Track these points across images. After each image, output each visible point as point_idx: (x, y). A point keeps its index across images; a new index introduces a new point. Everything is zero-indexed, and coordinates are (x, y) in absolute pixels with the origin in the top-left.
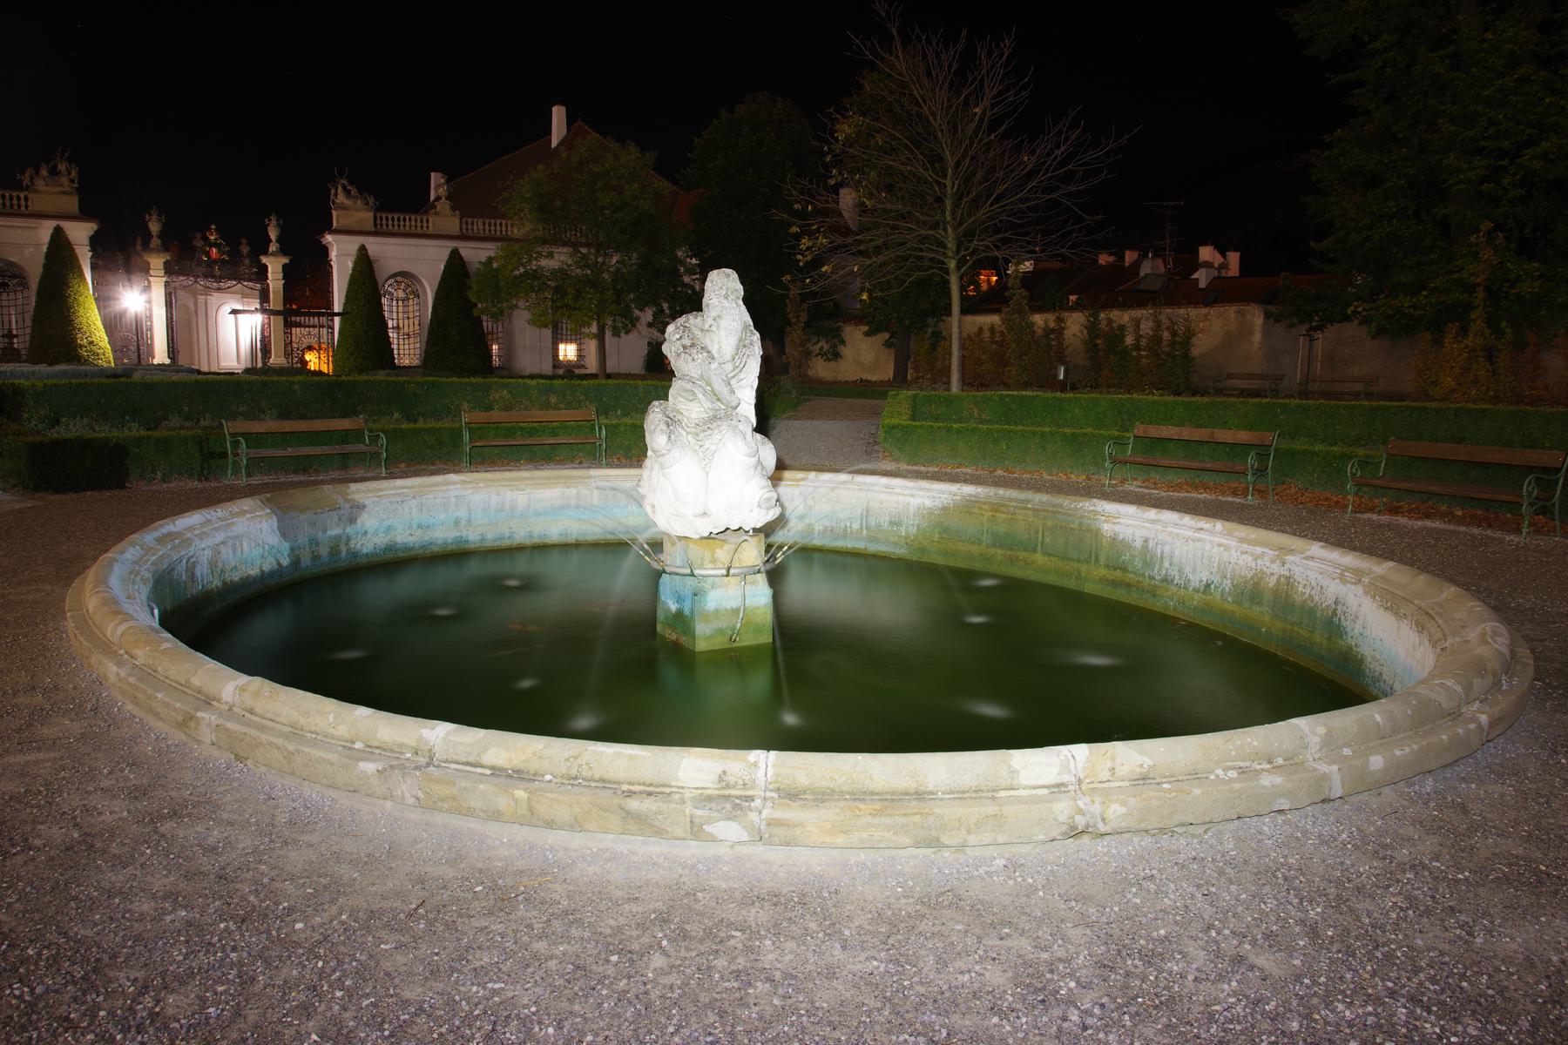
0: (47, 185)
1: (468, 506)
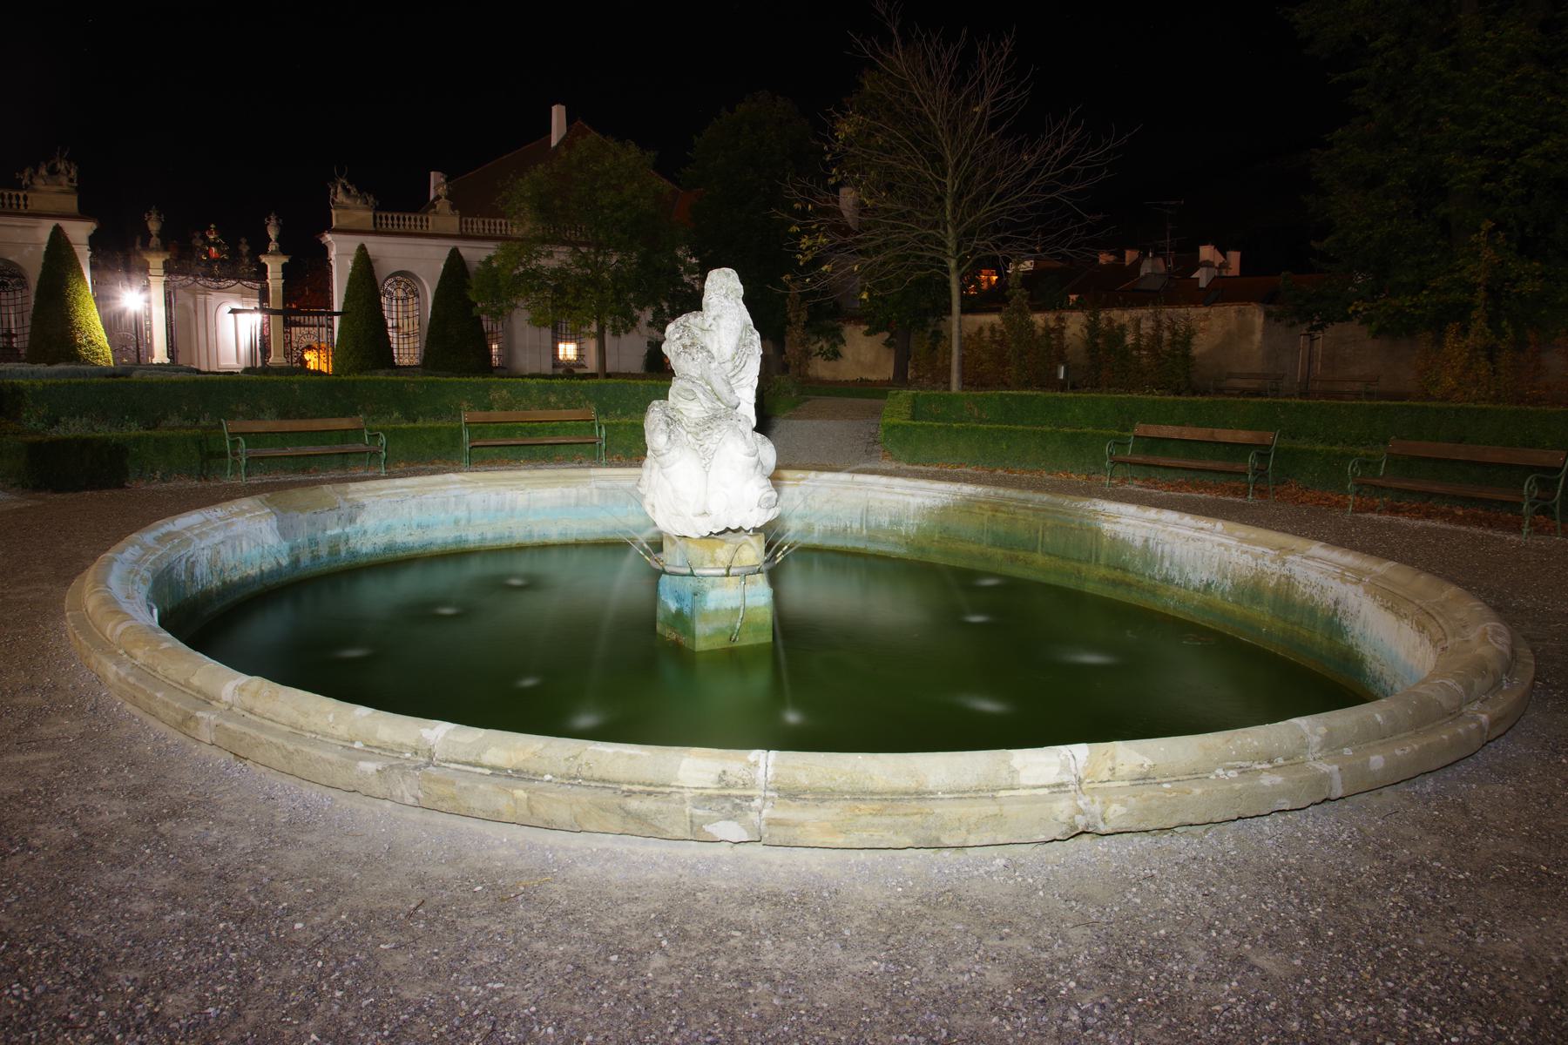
1: (468, 505)
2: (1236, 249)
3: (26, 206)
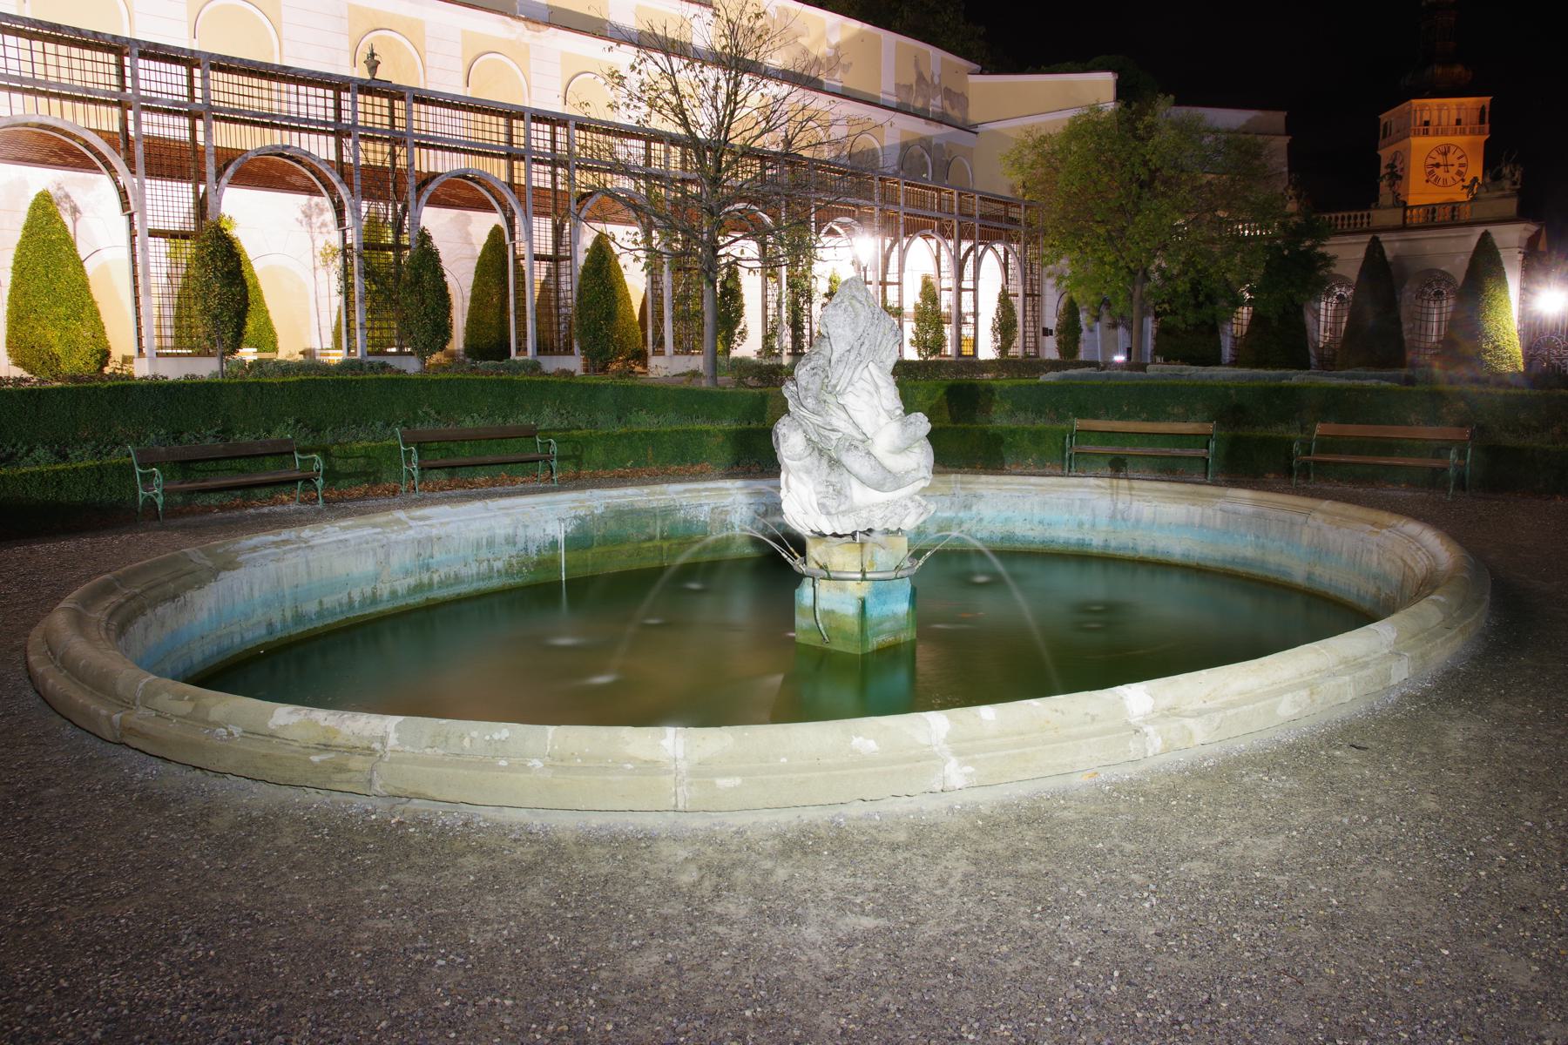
0: (1488, 191)
1: (1093, 510)
2: (1173, 94)
3: (1368, 223)
